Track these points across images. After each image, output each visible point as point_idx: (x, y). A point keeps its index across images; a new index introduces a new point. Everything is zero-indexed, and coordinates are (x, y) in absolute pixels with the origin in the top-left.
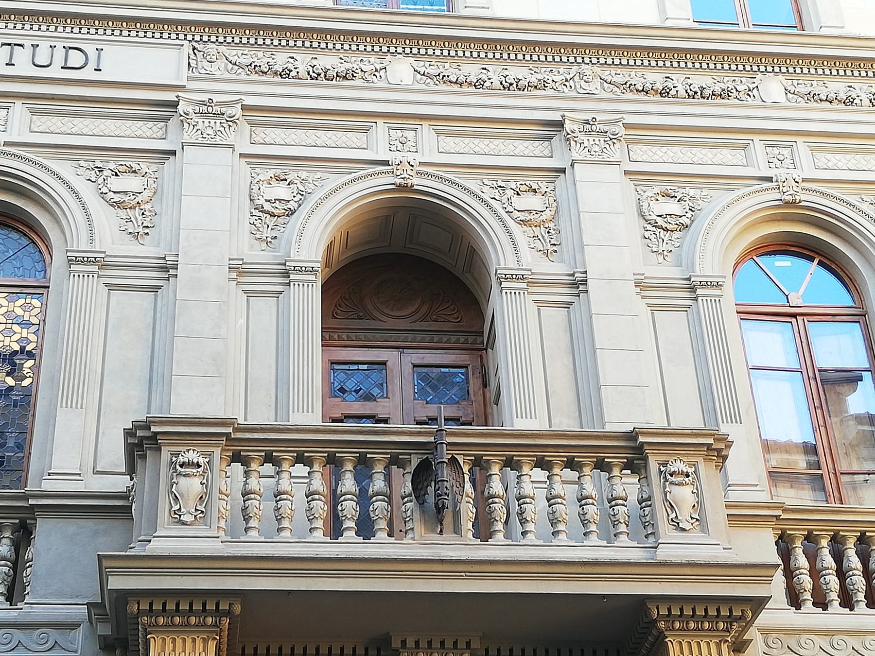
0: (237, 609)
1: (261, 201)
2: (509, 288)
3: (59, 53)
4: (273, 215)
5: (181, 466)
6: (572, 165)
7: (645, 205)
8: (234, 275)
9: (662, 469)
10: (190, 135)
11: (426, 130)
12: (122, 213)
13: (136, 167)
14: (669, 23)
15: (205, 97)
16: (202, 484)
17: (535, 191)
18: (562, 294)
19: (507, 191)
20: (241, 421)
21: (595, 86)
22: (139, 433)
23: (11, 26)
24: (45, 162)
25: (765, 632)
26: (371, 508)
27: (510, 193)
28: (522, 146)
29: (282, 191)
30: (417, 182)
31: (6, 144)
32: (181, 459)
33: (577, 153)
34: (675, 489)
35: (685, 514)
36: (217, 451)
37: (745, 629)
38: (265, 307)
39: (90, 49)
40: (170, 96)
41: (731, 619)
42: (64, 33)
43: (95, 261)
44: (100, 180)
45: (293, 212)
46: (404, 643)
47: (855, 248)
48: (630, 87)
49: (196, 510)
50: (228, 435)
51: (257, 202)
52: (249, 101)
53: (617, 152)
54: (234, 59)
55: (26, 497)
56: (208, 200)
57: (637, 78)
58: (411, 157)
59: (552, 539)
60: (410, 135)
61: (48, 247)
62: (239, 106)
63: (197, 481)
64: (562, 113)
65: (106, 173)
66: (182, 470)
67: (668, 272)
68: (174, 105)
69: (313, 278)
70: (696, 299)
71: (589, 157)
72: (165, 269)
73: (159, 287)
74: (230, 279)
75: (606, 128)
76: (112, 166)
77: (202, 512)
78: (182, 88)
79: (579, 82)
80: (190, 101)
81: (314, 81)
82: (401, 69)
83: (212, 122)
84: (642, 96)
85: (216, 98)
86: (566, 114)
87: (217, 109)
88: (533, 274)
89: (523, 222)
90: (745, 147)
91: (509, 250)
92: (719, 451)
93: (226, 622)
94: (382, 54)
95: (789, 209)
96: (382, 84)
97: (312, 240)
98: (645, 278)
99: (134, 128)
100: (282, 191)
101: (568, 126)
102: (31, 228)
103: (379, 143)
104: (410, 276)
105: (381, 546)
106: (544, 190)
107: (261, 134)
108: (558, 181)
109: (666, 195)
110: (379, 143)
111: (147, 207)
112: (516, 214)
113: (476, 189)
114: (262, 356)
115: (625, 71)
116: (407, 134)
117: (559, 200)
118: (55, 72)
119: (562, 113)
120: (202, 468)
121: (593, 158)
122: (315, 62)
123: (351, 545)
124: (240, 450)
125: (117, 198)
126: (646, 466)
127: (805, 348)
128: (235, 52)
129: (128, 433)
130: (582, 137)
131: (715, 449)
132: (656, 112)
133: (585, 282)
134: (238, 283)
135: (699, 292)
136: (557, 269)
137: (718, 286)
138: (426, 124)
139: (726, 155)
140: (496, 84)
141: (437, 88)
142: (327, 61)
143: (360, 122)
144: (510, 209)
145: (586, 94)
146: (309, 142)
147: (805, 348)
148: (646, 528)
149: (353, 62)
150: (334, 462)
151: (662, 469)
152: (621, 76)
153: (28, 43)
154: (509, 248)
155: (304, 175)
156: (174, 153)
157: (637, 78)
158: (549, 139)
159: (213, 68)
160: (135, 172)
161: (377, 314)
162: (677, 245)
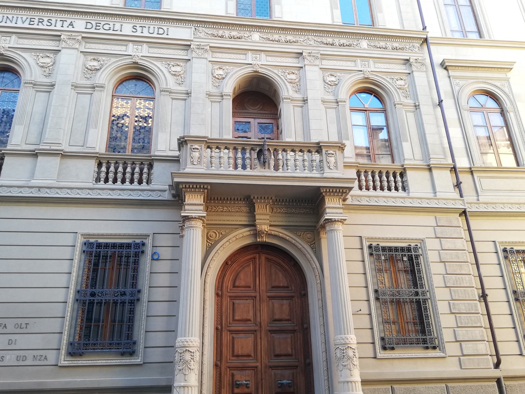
0: (209, 187)
1: (215, 75)
3: (156, 29)
4: (91, 70)
10: (64, 45)
11: (263, 54)
14: (335, 23)
15: (310, 51)
18: (300, 104)
21: (312, 42)
25: (352, 196)
27: (286, 74)
28: (290, 60)
30: (260, 70)
31: (9, 47)
32: (193, 147)
33: (306, 62)
35: (332, 165)
37: (346, 195)
39: (165, 28)
40: (188, 43)
41: (343, 192)
42: (157, 23)
43: (31, 83)
45: (224, 78)
46: (254, 197)
48: (213, 35)
55: (151, 156)
56: (200, 74)
57: (324, 40)
58: (138, 54)
65: (286, 74)
67: (214, 91)
68: (190, 46)
76: (172, 63)
78: (192, 41)
80: (194, 45)
82: (256, 36)
84: (326, 46)
85: (202, 44)
90: (355, 61)
91: (286, 91)
93: (206, 191)
94: (250, 31)
95: (366, 80)
96: (250, 41)
97: (229, 87)
101: (304, 54)
102: (150, 81)
103: (250, 58)
104: (257, 97)
105: (248, 172)
107: (88, 45)
109: (94, 59)
111: (50, 68)
114: (216, 119)
118: (155, 35)
123: (240, 171)
127: (368, 120)
129: (179, 140)
130: (308, 58)
132: (329, 50)
133: (307, 100)
136: (299, 96)
137: (345, 102)
138: (263, 53)
139: (349, 63)
140: (338, 45)
142: (234, 33)
143: (243, 52)
145: (308, 44)
147: (368, 120)
148: (321, 168)
149: (242, 34)
153: (147, 26)
154: (286, 90)
155: (227, 67)
159: (201, 35)
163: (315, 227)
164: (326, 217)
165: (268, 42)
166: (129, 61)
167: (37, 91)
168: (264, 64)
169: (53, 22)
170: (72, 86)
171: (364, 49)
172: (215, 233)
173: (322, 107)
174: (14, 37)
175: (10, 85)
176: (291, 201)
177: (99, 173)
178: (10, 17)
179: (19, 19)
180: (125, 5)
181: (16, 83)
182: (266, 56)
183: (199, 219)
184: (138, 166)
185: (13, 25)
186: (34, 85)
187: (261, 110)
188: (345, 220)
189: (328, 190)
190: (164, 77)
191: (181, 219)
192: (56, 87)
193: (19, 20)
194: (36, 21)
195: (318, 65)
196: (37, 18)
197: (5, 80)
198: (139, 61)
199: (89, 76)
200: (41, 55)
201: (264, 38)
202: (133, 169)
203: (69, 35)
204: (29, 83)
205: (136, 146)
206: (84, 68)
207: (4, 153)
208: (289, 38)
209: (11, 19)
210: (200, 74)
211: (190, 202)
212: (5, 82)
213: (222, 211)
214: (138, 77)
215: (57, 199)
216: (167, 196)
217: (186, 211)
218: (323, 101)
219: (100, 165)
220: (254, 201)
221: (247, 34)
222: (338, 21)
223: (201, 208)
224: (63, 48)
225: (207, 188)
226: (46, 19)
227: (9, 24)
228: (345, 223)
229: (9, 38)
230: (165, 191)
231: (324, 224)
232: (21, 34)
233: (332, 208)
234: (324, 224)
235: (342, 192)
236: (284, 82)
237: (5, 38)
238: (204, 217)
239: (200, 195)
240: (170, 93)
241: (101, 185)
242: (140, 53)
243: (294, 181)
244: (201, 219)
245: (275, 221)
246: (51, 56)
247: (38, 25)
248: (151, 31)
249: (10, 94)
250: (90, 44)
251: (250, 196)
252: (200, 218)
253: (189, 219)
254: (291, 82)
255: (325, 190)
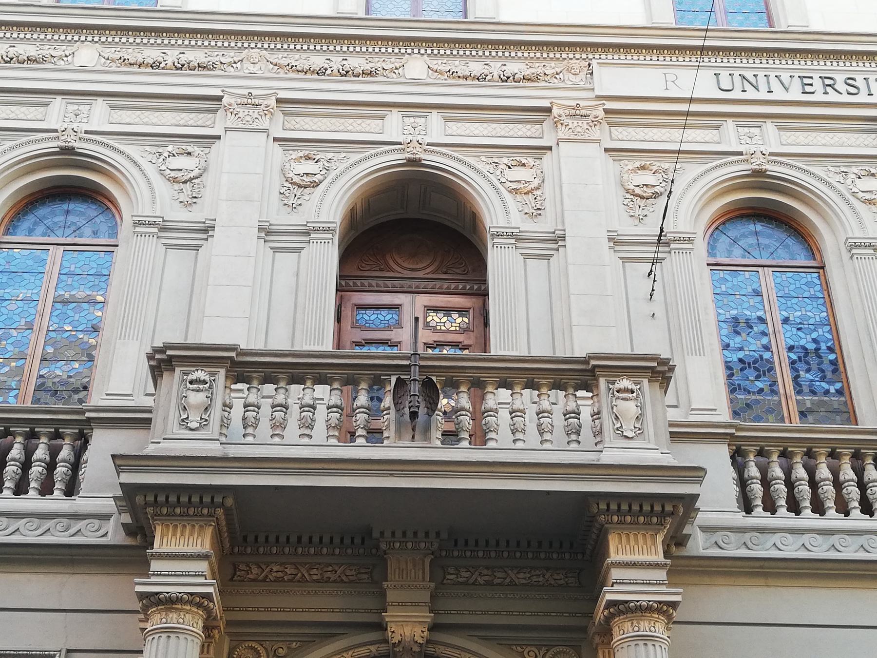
0: (230, 502)
1: (291, 175)
2: (677, 249)
4: (642, 198)
5: (618, 392)
6: (558, 144)
7: (626, 176)
8: (263, 235)
9: (611, 386)
10: (562, 133)
11: (435, 116)
12: (177, 186)
13: (524, 161)
15: (246, 92)
16: (207, 397)
17: (524, 165)
19: (849, 176)
20: (243, 346)
22: (158, 356)
23: (642, 58)
24: (116, 145)
25: (705, 529)
26: (483, 422)
29: (647, 178)
31: (86, 132)
32: (190, 377)
34: (619, 402)
36: (222, 372)
37: (682, 524)
38: (287, 260)
41: (663, 514)
43: (512, 236)
44: (498, 172)
45: (315, 185)
46: (382, 533)
47: (814, 209)
48: (452, 74)
49: (201, 418)
50: (231, 358)
51: (287, 175)
52: (282, 95)
53: (595, 133)
54: (435, 68)
55: (83, 412)
56: (244, 171)
57: (132, 54)
59: (524, 440)
60: (756, 131)
61: (119, 212)
62: (274, 98)
63: (631, 405)
64: (550, 101)
66: (191, 386)
69: (330, 236)
70: (670, 252)
71: (241, 126)
72: (205, 231)
73: (302, 248)
74: (259, 238)
75: (588, 113)
76: (505, 160)
77: (206, 420)
79: (246, 64)
81: (179, 71)
83: (580, 122)
86: (554, 101)
87: (584, 112)
88: (164, 221)
89: (516, 191)
91: (497, 211)
92: (663, 373)
93: (220, 511)
95: (759, 179)
98: (618, 235)
99: (498, 130)
100: (647, 178)
101: (556, 111)
102: (736, 217)
103: (393, 127)
104: (412, 230)
106: (532, 164)
107: (293, 121)
108: (545, 158)
110: (393, 127)
111: (538, 193)
112: (508, 184)
113: (823, 175)
114: (289, 299)
115: (304, 55)
116: (81, 107)
117: (545, 171)
119: (550, 101)
120: (208, 385)
121: (576, 137)
122: (504, 68)
123: (361, 450)
124: (534, 378)
125: (173, 174)
126: (597, 386)
128: (436, 62)
129: (150, 357)
131: (659, 372)
133: (563, 238)
134: (615, 251)
135: (672, 246)
137: (690, 240)
138: (769, 121)
140: (496, 77)
141: (119, 69)
144: (503, 180)
146: (638, 137)
149: (215, 56)
150: (377, 383)
151: (611, 386)
152: (278, 57)
156: (550, 148)
157: (459, 66)
158: (541, 122)
160: (524, 165)
161: (395, 267)
162: (652, 210)
163: (584, 630)
164: (609, 597)
165: (450, 81)
166: (53, 145)
167: (275, 250)
168: (431, 139)
169: (860, 82)
170: (260, 229)
171: (415, 82)
172: (252, 648)
173: (610, 258)
174: (770, 126)
175: (87, 230)
176: (337, 540)
177: (743, 483)
178: (749, 75)
179: (772, 79)
180: (367, 11)
181: (104, 228)
182: (447, 120)
183: (190, 602)
184: (19, 439)
185: (763, 95)
186: (163, 229)
187: (433, 272)
188: (674, 605)
189: (613, 507)
190: (143, 187)
191: (138, 606)
192: (217, 232)
193: (775, 85)
194: (818, 85)
195: (598, 141)
196: (816, 76)
197: (71, 218)
198: (423, 156)
199: (638, 212)
200: (505, 160)
201: (280, 66)
202: (54, 452)
203: (244, 96)
204: (150, 224)
205: (808, 405)
206: (622, 192)
207: (89, 420)
208: (514, 68)
209: (753, 80)
210: (244, 171)
211: (165, 549)
212: (73, 223)
213: (277, 580)
214: (766, 211)
215: (837, 565)
216: (112, 533)
217: (153, 579)
218: (616, 241)
219: (738, 457)
220: (383, 546)
221: (230, 56)
222: (666, 16)
223: (203, 566)
224: (227, 130)
225: (222, 505)
226: (840, 78)
227: (751, 94)
228: (676, 615)
229: (88, 107)
230: (106, 517)
231: (608, 619)
232: (787, 118)
233: (633, 565)
234: (608, 619)
235: (668, 514)
236: (847, 201)
237: (76, 107)
238: (208, 596)
239: (644, 535)
240: (519, 239)
241: (760, 517)
242: (766, 144)
243: (466, 475)
244: (199, 605)
245: (498, 613)
246: (531, 161)
247: (826, 93)
248: (726, 84)
249: (796, 276)
250: (298, 119)
251: (369, 532)
252: (198, 601)
253: (630, 610)
254: (516, 191)
255: (603, 506)
